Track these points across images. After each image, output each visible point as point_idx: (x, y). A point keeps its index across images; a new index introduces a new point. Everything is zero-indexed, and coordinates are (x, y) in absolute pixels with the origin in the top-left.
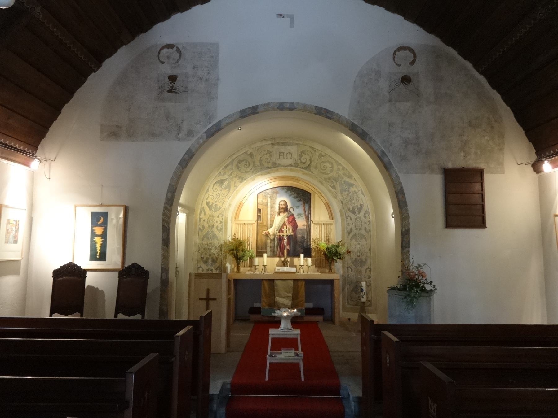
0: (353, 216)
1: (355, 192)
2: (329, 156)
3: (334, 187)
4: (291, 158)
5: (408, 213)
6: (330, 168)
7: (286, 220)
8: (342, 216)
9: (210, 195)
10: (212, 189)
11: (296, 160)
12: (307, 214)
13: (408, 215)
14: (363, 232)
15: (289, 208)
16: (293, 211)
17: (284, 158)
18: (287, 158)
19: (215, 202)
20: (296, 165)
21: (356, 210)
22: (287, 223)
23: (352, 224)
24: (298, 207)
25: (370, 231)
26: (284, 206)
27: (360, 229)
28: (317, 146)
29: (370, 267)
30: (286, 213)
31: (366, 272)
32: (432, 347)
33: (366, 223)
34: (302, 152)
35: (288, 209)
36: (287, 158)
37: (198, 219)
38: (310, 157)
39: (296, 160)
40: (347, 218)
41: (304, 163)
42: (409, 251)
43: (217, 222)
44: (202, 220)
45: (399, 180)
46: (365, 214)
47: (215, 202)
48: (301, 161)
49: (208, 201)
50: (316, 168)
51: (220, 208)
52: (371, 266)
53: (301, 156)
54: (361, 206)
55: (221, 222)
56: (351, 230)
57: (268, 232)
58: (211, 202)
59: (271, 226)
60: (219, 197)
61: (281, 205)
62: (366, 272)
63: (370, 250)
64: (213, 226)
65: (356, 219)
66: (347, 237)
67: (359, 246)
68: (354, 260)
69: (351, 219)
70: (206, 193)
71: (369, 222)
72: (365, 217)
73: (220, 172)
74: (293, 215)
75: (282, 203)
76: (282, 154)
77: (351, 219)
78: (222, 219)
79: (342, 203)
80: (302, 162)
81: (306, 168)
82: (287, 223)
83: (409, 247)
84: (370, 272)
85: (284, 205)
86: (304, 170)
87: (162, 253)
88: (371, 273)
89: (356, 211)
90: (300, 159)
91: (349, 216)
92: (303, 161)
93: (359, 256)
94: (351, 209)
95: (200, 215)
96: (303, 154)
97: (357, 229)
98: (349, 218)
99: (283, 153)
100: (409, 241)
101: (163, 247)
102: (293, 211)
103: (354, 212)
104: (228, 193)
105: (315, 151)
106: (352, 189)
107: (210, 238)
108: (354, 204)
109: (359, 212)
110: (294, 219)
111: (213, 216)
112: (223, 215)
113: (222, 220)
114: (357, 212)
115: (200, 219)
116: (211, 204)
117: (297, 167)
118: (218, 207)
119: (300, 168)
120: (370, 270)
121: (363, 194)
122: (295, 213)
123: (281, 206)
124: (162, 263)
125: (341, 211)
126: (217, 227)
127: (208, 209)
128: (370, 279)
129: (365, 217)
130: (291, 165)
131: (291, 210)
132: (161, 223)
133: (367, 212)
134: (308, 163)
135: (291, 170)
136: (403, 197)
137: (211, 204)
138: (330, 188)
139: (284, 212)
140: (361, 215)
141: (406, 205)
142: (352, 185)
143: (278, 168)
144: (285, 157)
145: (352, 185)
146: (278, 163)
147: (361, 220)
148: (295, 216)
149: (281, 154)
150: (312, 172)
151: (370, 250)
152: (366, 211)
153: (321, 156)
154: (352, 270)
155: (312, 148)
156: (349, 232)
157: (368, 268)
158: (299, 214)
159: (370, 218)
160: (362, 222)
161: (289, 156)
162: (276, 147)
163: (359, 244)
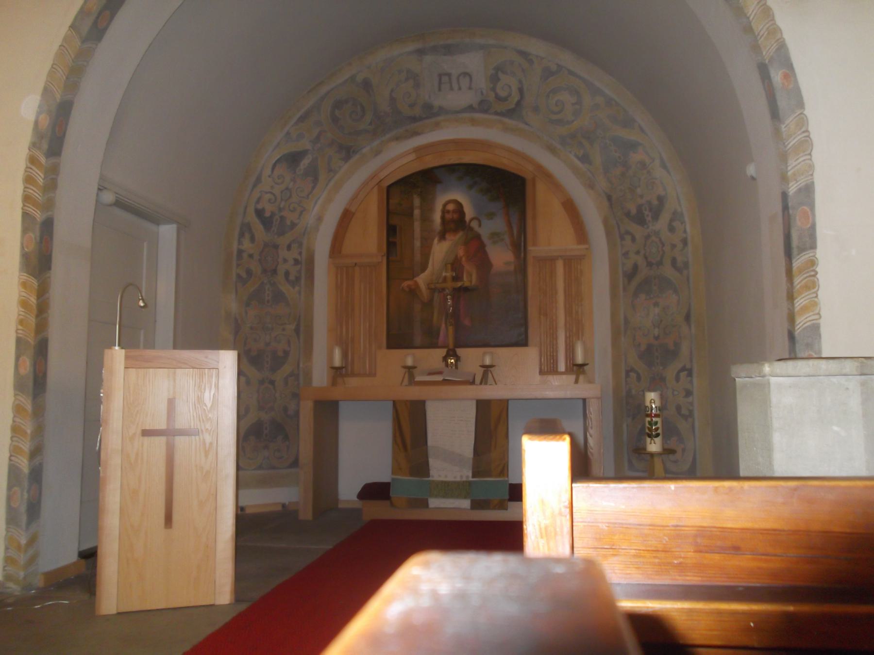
0: (638, 231)
1: (643, 165)
2: (571, 73)
3: (585, 159)
4: (470, 88)
5: (807, 131)
6: (573, 104)
7: (461, 252)
8: (608, 233)
9: (267, 193)
10: (269, 176)
11: (484, 92)
12: (515, 232)
13: (808, 136)
14: (668, 271)
15: (468, 218)
16: (480, 225)
17: (452, 89)
18: (460, 89)
19: (280, 210)
20: (483, 107)
21: (646, 213)
22: (464, 259)
23: (638, 253)
24: (491, 216)
25: (686, 265)
26: (455, 216)
27: (660, 263)
28: (537, 48)
29: (688, 366)
30: (460, 234)
31: (677, 379)
32: (101, 411)
33: (674, 246)
34: (499, 69)
35: (465, 222)
36: (460, 89)
37: (235, 253)
38: (520, 82)
39: (482, 93)
40: (622, 238)
41: (505, 99)
42: (813, 263)
43: (285, 261)
44: (245, 255)
45: (773, 19)
46: (672, 220)
47: (280, 210)
48: (496, 94)
49: (260, 207)
50: (536, 109)
51: (293, 225)
52: (691, 361)
53: (494, 79)
54: (661, 200)
55: (297, 262)
56: (635, 268)
57: (416, 284)
58: (269, 209)
59: (424, 268)
60: (290, 197)
61: (448, 212)
62: (677, 379)
63: (688, 318)
64: (275, 272)
65: (648, 237)
66: (625, 289)
67: (657, 310)
68: (643, 347)
69: (633, 239)
70: (255, 186)
71: (685, 242)
72: (672, 229)
73: (288, 133)
74: (478, 237)
75: (451, 207)
76: (445, 79)
77: (633, 239)
78: (300, 253)
79: (609, 198)
80: (498, 98)
81: (510, 113)
82: (464, 259)
83: (813, 246)
84: (689, 379)
85: (454, 211)
86: (506, 120)
87: (20, 296)
88: (691, 382)
89: (648, 216)
90: (493, 89)
91: (628, 233)
92: (503, 94)
93: (657, 338)
94: (634, 211)
95: (240, 243)
96: (500, 75)
97: (650, 264)
98: (628, 238)
99: (449, 75)
100: (813, 227)
101: (25, 277)
102: (480, 225)
103: (640, 219)
104: (313, 188)
105: (531, 62)
106: (636, 157)
107: (268, 301)
108: (641, 197)
109: (656, 216)
110: (482, 247)
111: (276, 247)
112: (300, 245)
113: (298, 257)
114: (649, 219)
115: (240, 252)
116: (267, 214)
117: (486, 111)
118: (288, 223)
119: (496, 113)
120: (690, 374)
121: (664, 166)
122: (485, 229)
123: (448, 216)
124: (20, 327)
125: (605, 222)
126: (287, 274)
127: (261, 227)
128: (690, 399)
129: (672, 229)
130: (470, 108)
131: (474, 224)
132: (19, 204)
133: (676, 216)
134: (515, 98)
135: (474, 122)
136: (786, 76)
137: (267, 214)
138: (577, 162)
139: (455, 231)
140: (661, 225)
141: (801, 104)
142: (633, 146)
143: (440, 118)
144: (455, 86)
145: (633, 146)
146: (437, 103)
147: (660, 240)
148: (485, 238)
149: (444, 79)
150: (527, 124)
151: (688, 318)
152: (675, 213)
153: (548, 73)
154: (639, 378)
155: (523, 54)
156: (630, 276)
157: (683, 369)
158: (495, 236)
159: (685, 231)
160: (663, 245)
161: (465, 82)
162: (428, 58)
163: (656, 304)
